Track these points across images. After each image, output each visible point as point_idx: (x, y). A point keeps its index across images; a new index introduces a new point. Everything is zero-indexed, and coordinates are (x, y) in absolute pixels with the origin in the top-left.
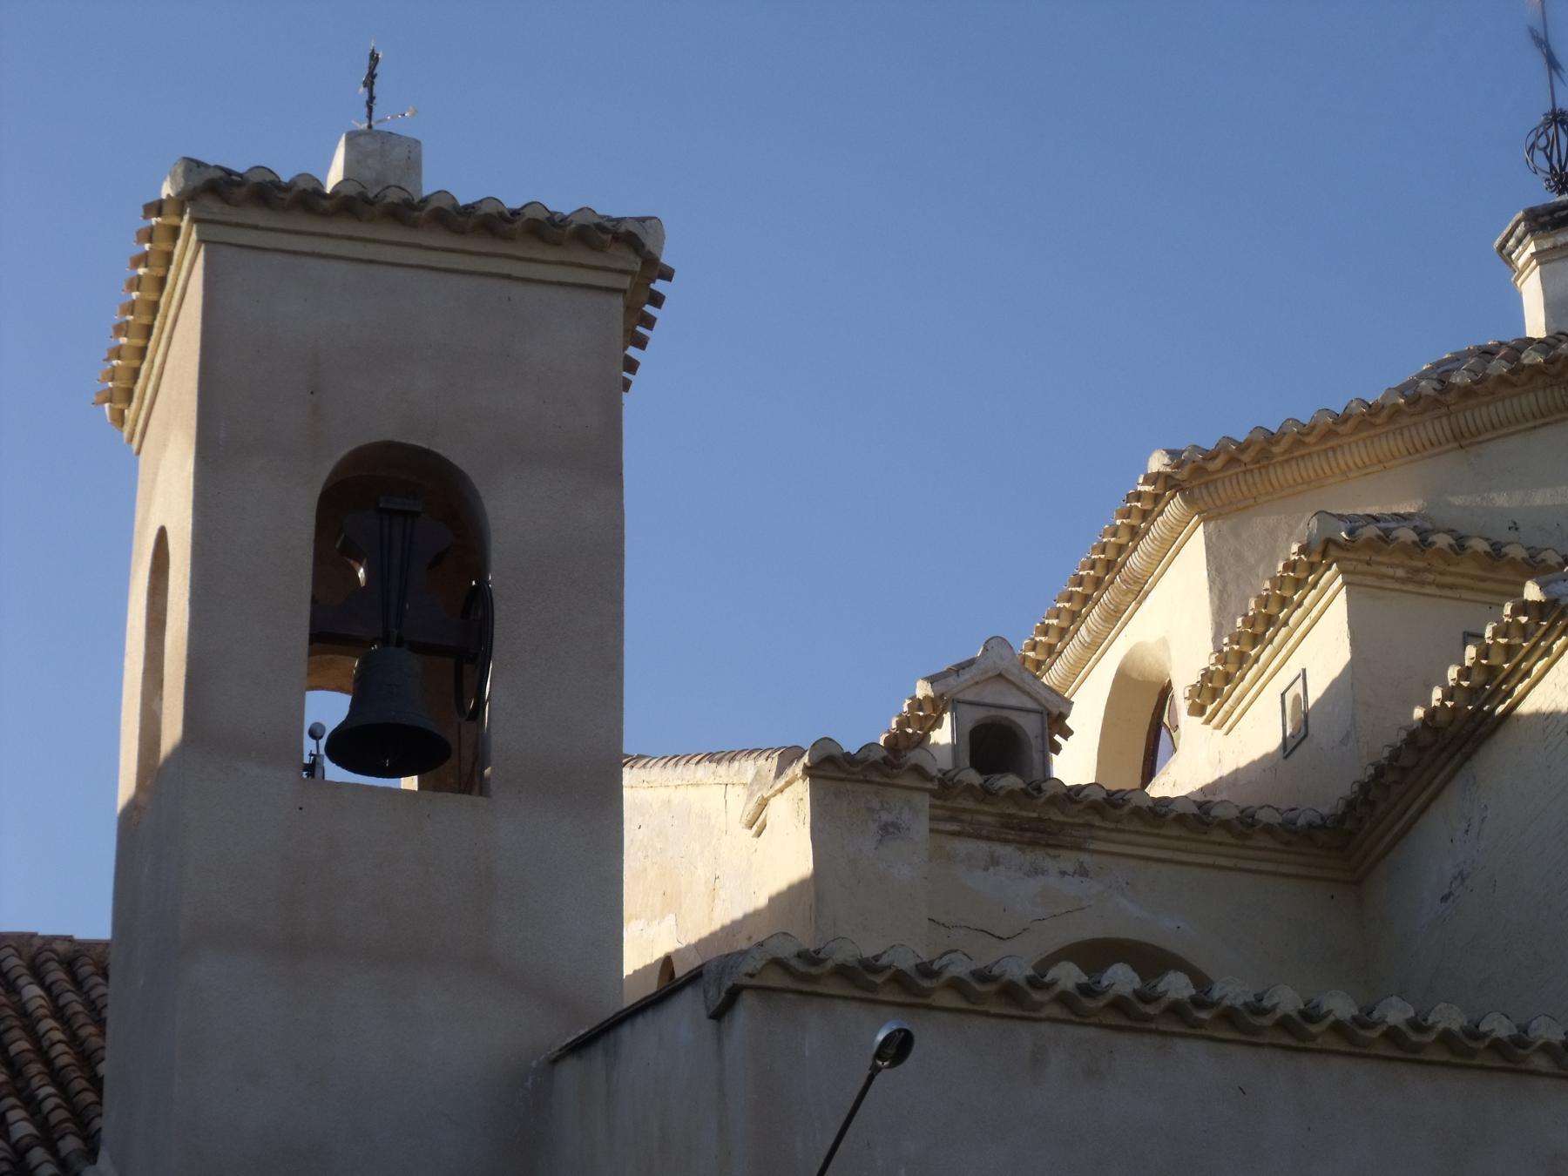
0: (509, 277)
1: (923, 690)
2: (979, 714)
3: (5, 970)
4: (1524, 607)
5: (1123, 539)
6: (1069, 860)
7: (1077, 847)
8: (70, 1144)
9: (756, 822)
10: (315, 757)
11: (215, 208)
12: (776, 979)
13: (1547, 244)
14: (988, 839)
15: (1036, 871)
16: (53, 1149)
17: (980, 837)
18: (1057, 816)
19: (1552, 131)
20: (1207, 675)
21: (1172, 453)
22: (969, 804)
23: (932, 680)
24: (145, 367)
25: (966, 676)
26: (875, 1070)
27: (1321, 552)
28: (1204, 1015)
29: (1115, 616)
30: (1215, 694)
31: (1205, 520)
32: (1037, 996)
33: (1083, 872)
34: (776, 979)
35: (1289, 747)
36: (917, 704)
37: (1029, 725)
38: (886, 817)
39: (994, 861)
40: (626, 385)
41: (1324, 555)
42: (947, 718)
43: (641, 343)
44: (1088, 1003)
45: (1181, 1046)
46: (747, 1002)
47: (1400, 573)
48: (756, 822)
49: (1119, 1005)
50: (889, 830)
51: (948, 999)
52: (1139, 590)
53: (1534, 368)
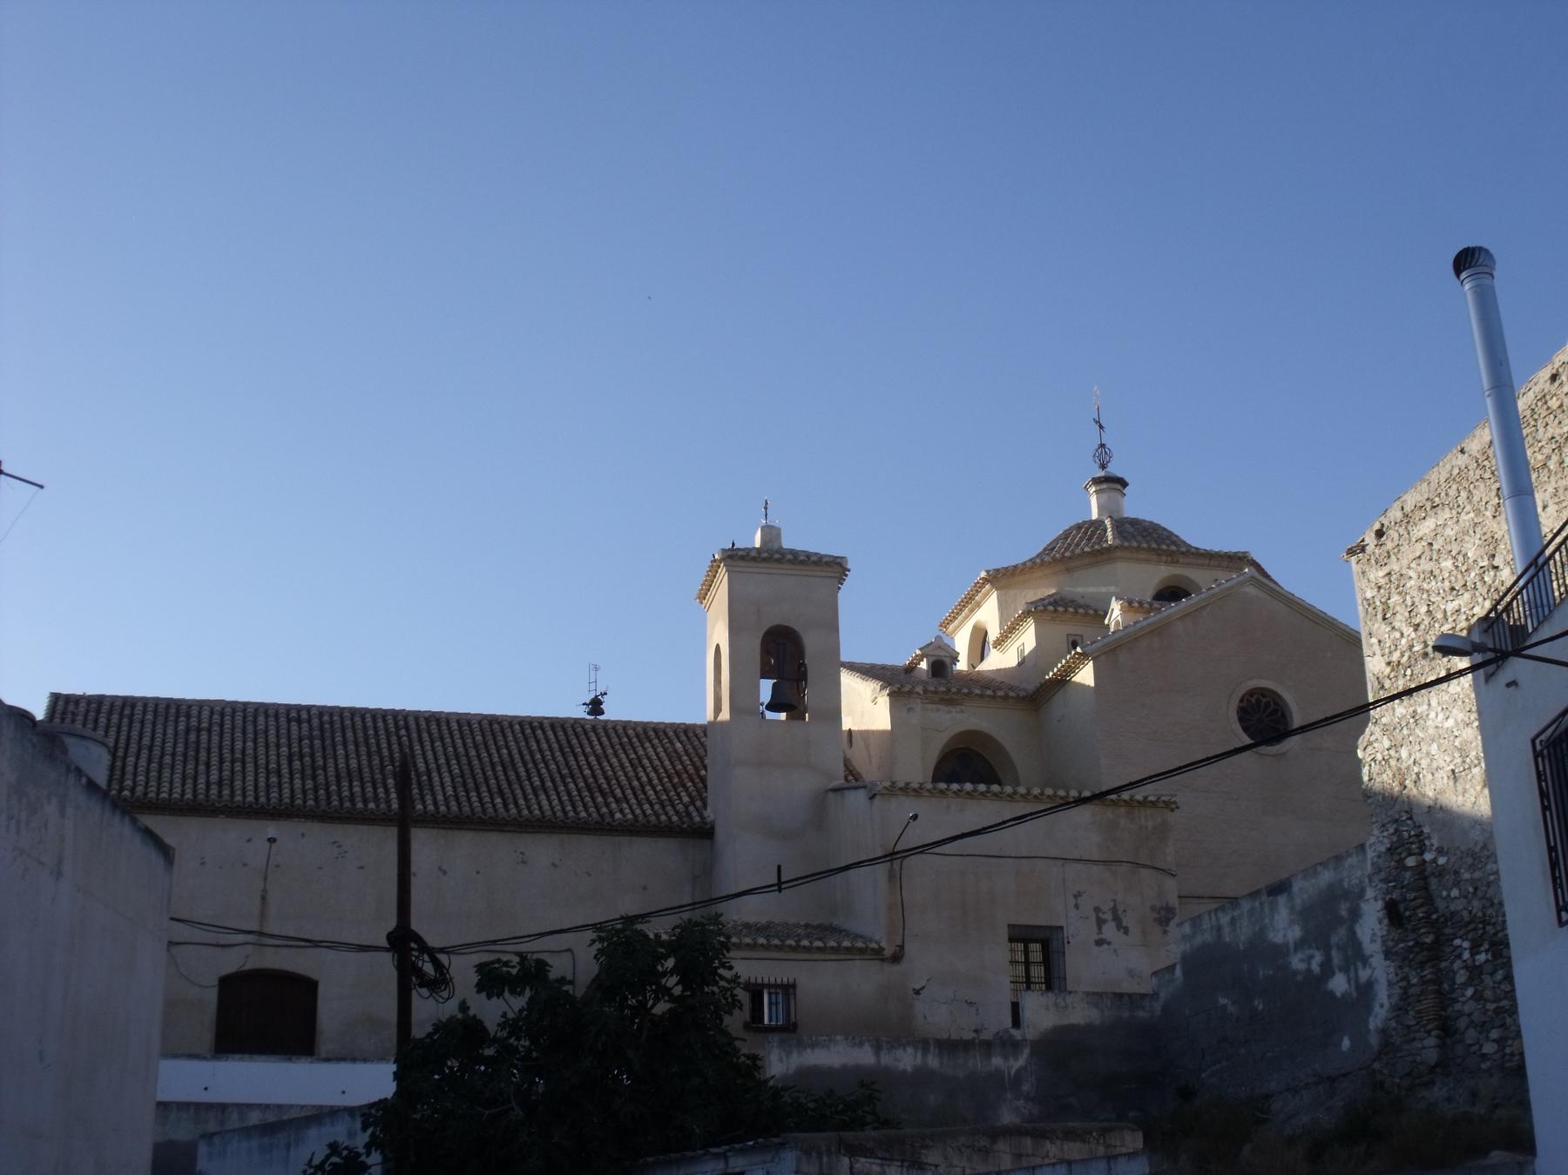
0: (807, 576)
1: (918, 652)
2: (935, 658)
3: (786, 983)
4: (1077, 653)
5: (974, 592)
6: (958, 708)
7: (962, 705)
8: (699, 803)
9: (874, 701)
10: (763, 711)
11: (730, 562)
12: (885, 792)
13: (1098, 488)
14: (936, 704)
15: (950, 712)
16: (695, 806)
17: (933, 703)
18: (955, 697)
19: (1100, 450)
20: (998, 639)
21: (988, 572)
22: (931, 695)
23: (920, 649)
24: (709, 593)
25: (930, 647)
26: (909, 822)
27: (1027, 614)
28: (989, 795)
29: (972, 611)
30: (1000, 644)
31: (996, 590)
32: (948, 792)
33: (962, 712)
34: (885, 792)
35: (1020, 664)
36: (917, 656)
37: (947, 661)
38: (909, 706)
39: (938, 710)
40: (839, 588)
41: (1028, 614)
42: (925, 659)
43: (842, 584)
44: (961, 794)
45: (983, 801)
46: (878, 797)
47: (1049, 618)
48: (874, 701)
49: (968, 793)
50: (910, 710)
51: (927, 794)
52: (979, 605)
53: (1088, 553)
